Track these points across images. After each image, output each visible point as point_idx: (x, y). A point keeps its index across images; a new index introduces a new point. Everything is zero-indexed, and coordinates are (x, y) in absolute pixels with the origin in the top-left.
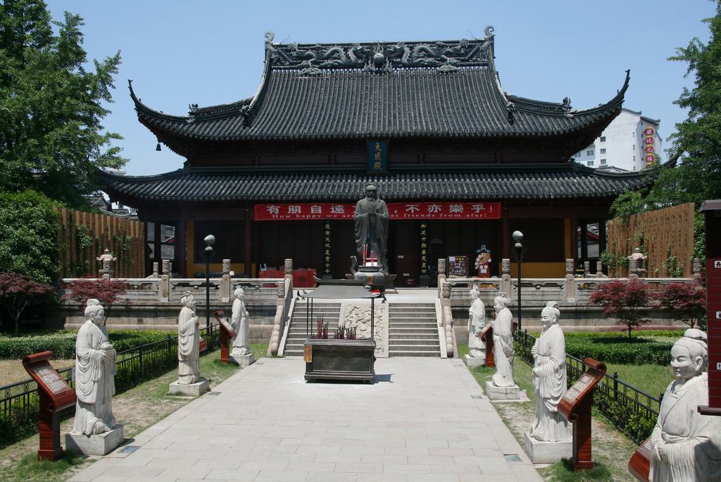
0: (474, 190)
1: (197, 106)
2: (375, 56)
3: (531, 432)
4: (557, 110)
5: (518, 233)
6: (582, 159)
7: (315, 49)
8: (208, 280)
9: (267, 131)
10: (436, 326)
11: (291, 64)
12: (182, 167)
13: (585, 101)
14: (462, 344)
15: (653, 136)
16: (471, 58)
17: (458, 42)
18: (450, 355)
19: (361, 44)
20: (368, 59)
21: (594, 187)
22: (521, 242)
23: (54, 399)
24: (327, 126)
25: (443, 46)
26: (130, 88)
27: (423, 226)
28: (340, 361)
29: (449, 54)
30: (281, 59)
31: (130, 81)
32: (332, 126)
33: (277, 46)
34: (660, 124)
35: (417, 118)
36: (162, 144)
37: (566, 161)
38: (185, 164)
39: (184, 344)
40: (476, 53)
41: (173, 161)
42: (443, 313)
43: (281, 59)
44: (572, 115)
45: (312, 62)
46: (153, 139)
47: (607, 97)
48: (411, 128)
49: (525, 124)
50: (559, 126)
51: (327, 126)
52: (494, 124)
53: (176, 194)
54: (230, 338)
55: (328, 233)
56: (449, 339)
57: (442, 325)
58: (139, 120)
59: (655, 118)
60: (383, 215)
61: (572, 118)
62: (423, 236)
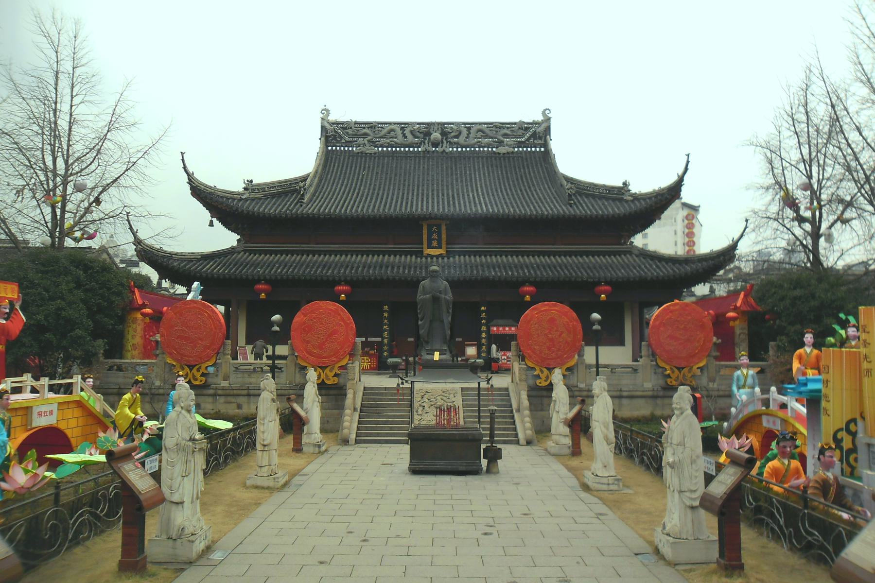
0: (535, 272)
1: (251, 181)
2: (432, 137)
3: (664, 528)
4: (619, 193)
5: (596, 316)
6: (638, 241)
7: (371, 127)
8: (274, 362)
9: (325, 209)
10: (512, 412)
11: (347, 142)
12: (235, 244)
13: (645, 182)
14: (543, 429)
15: (694, 221)
16: (528, 140)
17: (515, 124)
18: (529, 443)
19: (419, 124)
20: (425, 139)
21: (655, 270)
22: (599, 324)
23: (142, 498)
24: (385, 206)
25: (500, 128)
26: (183, 160)
27: (483, 308)
28: (448, 453)
29: (506, 135)
30: (334, 134)
31: (182, 154)
32: (390, 206)
33: (333, 123)
34: (700, 209)
35: (481, 200)
36: (215, 220)
37: (625, 243)
38: (238, 241)
39: (263, 432)
40: (537, 134)
41: (225, 239)
42: (520, 399)
43: (334, 134)
44: (630, 198)
45: (369, 141)
46: (206, 214)
47: (666, 181)
48: (471, 209)
49: (586, 208)
50: (618, 209)
51: (385, 206)
52: (551, 207)
53: (229, 271)
54: (304, 424)
55: (386, 315)
56: (528, 425)
57: (518, 410)
58: (192, 194)
59: (695, 204)
60: (447, 297)
61: (632, 201)
62: (483, 318)
